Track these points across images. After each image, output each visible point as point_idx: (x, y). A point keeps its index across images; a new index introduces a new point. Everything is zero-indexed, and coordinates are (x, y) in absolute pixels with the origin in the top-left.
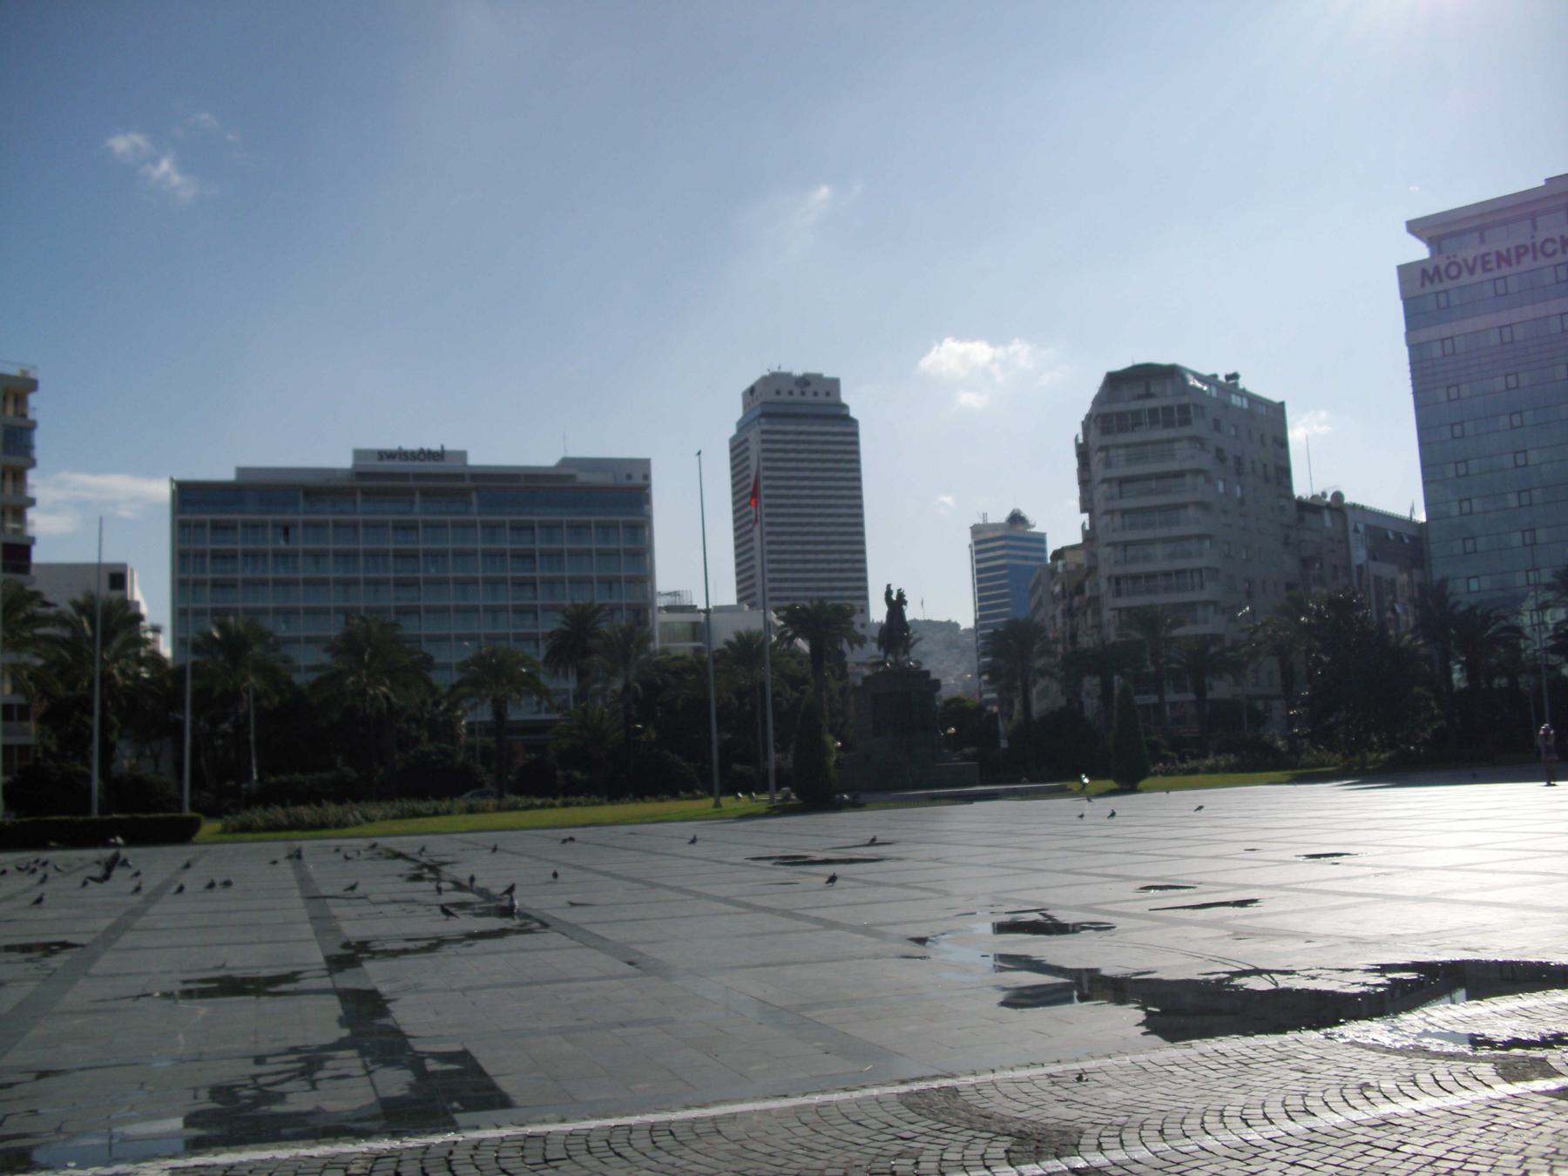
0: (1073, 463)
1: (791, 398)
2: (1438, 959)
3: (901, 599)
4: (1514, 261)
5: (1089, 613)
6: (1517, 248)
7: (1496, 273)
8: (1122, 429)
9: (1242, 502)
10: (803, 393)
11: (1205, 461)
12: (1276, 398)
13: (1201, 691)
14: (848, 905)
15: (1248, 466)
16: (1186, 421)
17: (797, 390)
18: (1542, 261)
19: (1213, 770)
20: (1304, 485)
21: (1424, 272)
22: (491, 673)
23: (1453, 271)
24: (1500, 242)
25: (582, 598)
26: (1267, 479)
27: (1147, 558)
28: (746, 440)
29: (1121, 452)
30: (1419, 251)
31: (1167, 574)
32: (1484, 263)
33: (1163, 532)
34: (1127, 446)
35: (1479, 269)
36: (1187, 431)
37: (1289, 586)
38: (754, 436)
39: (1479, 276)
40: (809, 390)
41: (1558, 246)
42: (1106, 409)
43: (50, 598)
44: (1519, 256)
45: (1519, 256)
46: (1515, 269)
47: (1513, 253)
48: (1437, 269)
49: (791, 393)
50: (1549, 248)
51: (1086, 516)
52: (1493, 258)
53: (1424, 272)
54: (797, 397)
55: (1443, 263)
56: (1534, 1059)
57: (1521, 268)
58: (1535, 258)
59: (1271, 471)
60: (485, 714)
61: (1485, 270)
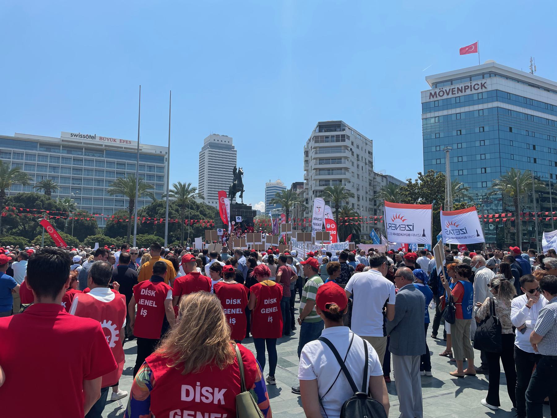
4: (463, 91)
7: (457, 95)
14: (449, 394)
16: (344, 141)
18: (474, 91)
21: (431, 94)
23: (441, 94)
32: (453, 91)
35: (451, 93)
38: (207, 152)
43: (436, 343)
45: (465, 89)
48: (435, 93)
52: (456, 90)
53: (431, 94)
57: (466, 94)
58: (471, 90)
61: (453, 94)
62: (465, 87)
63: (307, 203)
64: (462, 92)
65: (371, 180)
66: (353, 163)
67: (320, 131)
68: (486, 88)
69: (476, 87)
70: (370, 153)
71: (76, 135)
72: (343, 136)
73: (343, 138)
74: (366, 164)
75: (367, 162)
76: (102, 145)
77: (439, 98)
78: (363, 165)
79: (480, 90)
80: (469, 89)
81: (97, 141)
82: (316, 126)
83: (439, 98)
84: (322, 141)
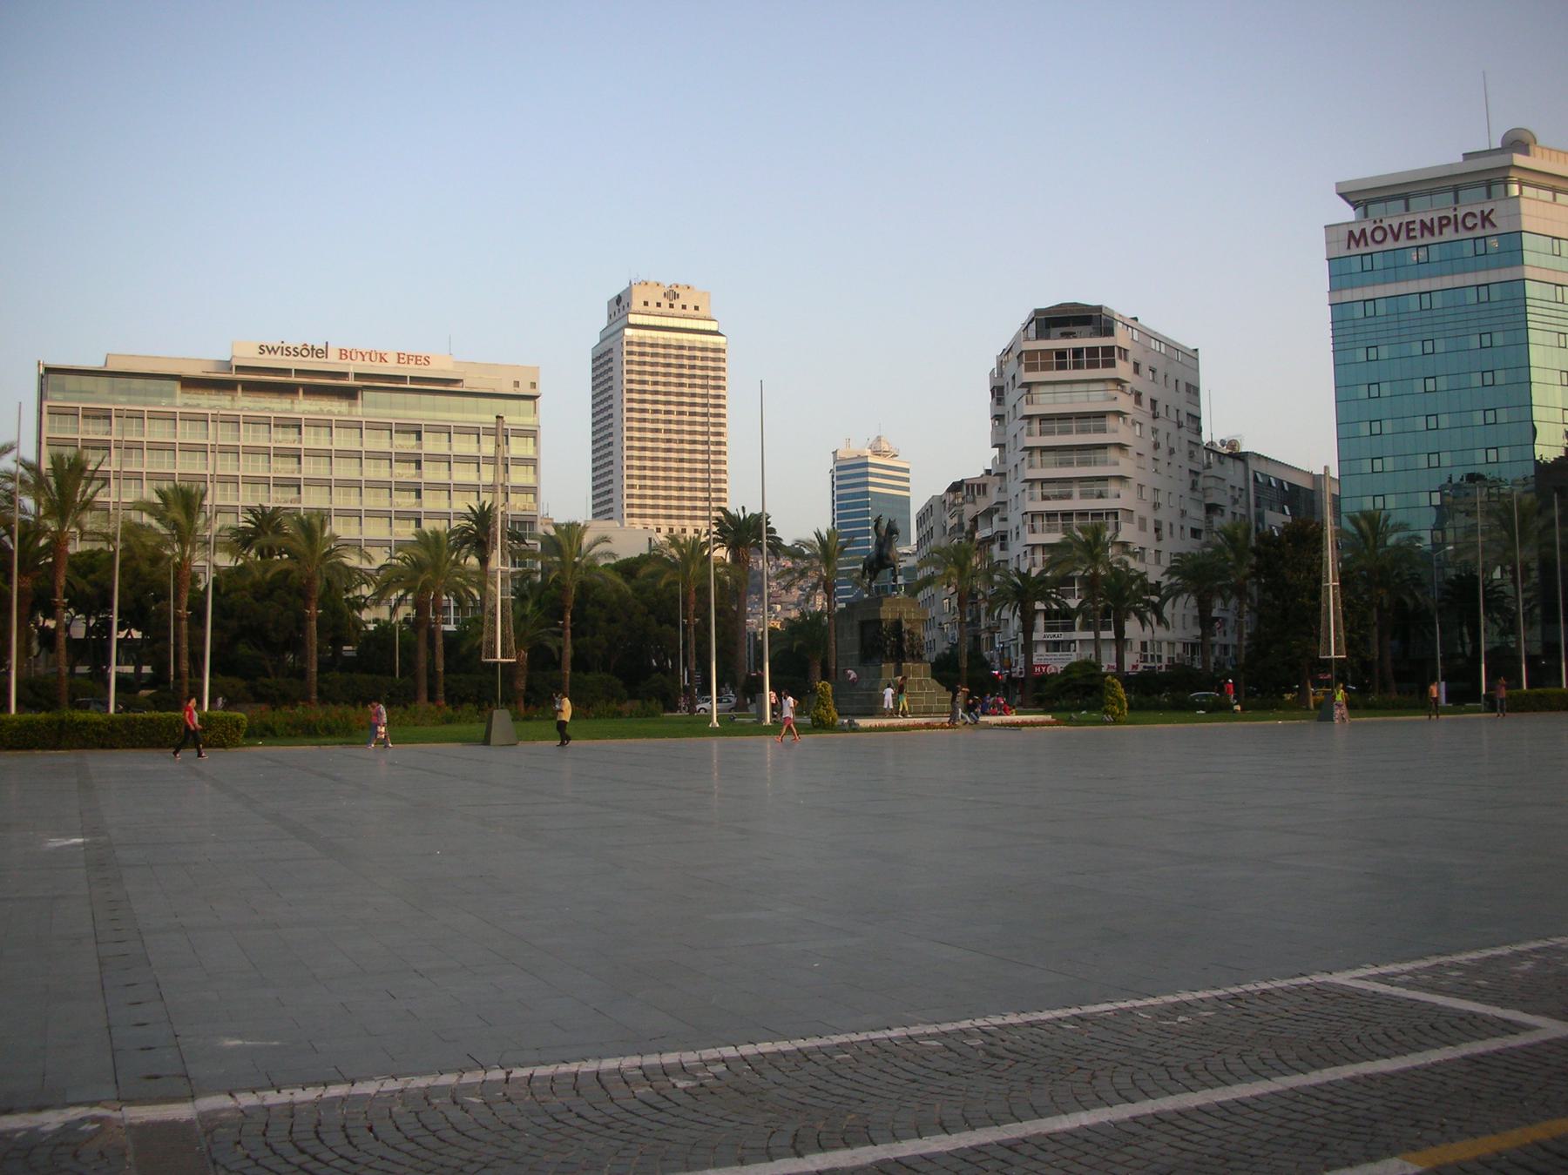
2: (632, 741)
4: (1436, 230)
6: (1440, 219)
7: (1420, 242)
10: (671, 306)
12: (1187, 341)
16: (1111, 364)
17: (665, 303)
18: (1463, 234)
19: (1159, 707)
20: (1214, 430)
21: (1351, 233)
23: (1379, 236)
24: (1424, 211)
25: (186, 466)
28: (610, 350)
30: (1346, 214)
32: (1409, 230)
35: (1403, 235)
39: (1403, 242)
40: (678, 304)
44: (1441, 227)
45: (1441, 227)
47: (1436, 224)
48: (1363, 232)
49: (659, 305)
50: (1469, 223)
52: (1417, 226)
53: (1351, 233)
55: (1369, 228)
61: (1409, 238)
62: (1440, 219)
63: (1003, 548)
64: (1432, 234)
65: (1197, 474)
66: (1138, 395)
67: (1041, 334)
68: (1493, 225)
69: (1469, 223)
70: (1193, 390)
71: (273, 350)
72: (1109, 351)
73: (1108, 356)
74: (1180, 426)
75: (1183, 418)
76: (344, 375)
77: (1373, 248)
78: (1172, 428)
79: (1479, 232)
80: (1452, 227)
81: (333, 363)
82: (1024, 317)
83: (1373, 248)
84: (1046, 367)
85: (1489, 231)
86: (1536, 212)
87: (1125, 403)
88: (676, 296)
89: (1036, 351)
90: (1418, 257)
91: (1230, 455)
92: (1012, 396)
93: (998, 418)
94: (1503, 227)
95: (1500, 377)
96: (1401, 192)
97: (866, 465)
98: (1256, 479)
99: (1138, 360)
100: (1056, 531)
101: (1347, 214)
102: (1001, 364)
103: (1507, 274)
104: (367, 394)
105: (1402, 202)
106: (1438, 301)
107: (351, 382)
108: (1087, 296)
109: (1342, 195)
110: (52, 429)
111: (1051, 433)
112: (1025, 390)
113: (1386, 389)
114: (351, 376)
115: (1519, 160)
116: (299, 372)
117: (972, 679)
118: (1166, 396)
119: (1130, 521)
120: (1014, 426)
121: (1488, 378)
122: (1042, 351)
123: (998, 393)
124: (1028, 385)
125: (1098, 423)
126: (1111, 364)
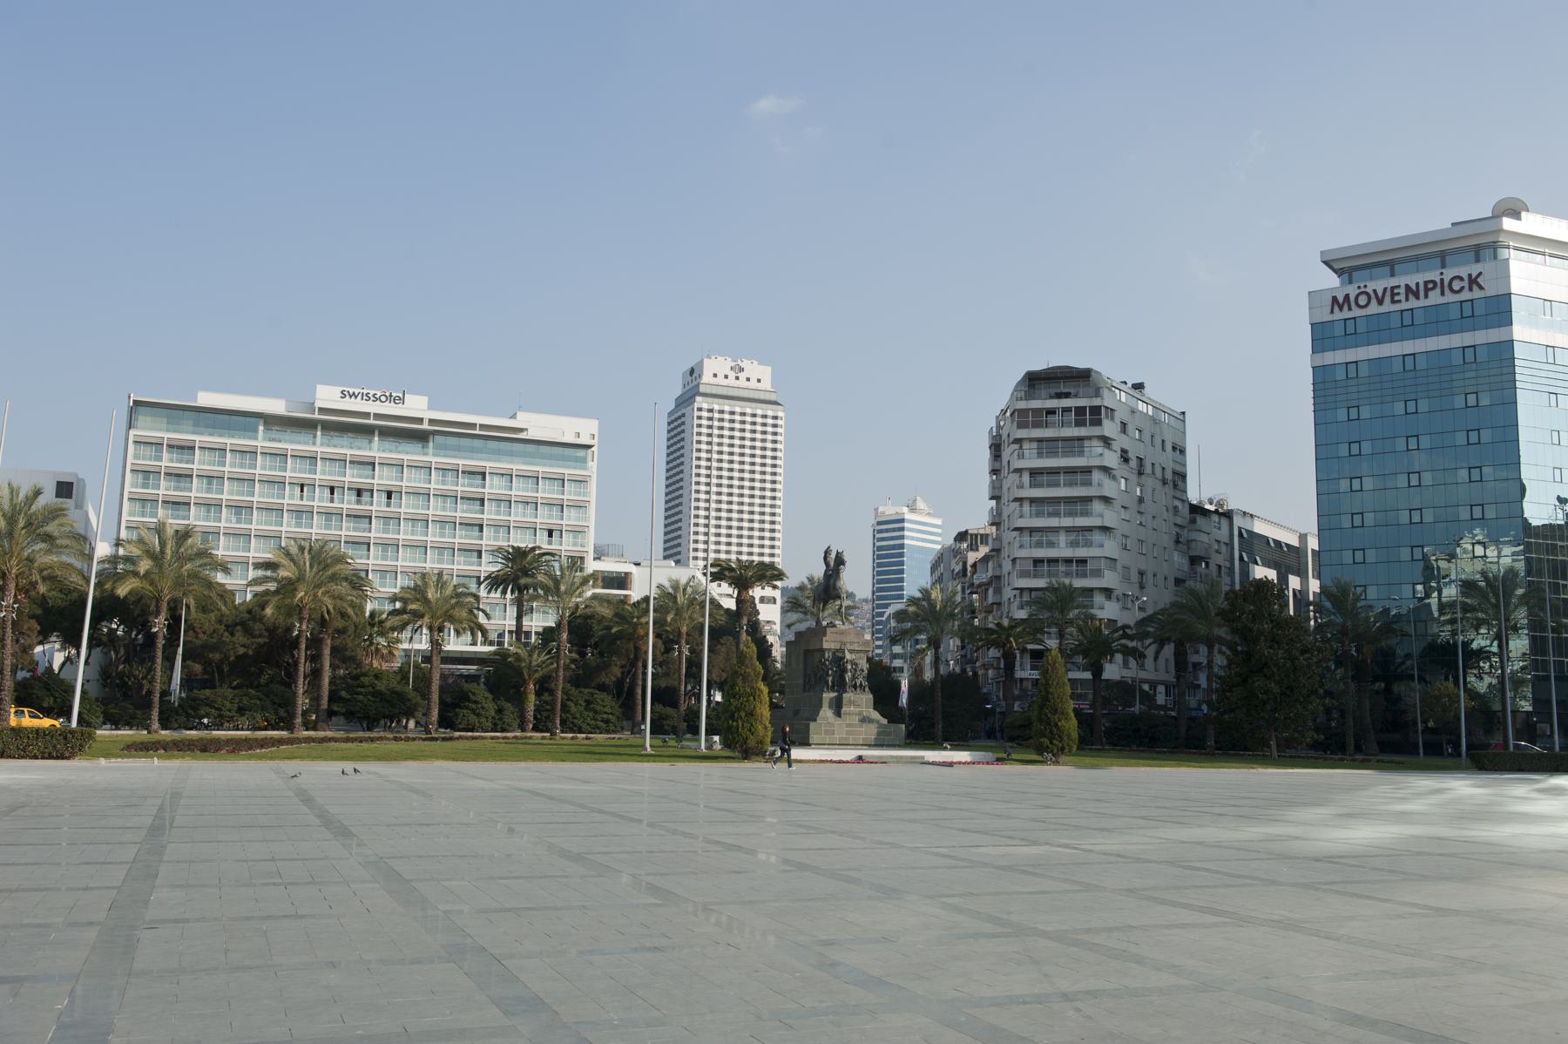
0: (986, 454)
1: (725, 382)
3: (840, 561)
4: (1422, 294)
5: (991, 591)
6: (1426, 283)
7: (1404, 306)
8: (1037, 425)
9: (1141, 500)
11: (1111, 459)
13: (1097, 671)
15: (1148, 469)
17: (732, 375)
18: (1450, 297)
20: (1196, 492)
21: (1335, 299)
22: (428, 604)
23: (1363, 300)
26: (1164, 482)
27: (1051, 545)
29: (1035, 445)
31: (1068, 561)
32: (1393, 295)
33: (1067, 522)
34: (1039, 440)
35: (1387, 299)
36: (1095, 431)
37: (1178, 582)
40: (742, 376)
41: (1466, 284)
42: (1022, 405)
44: (1427, 290)
45: (1427, 290)
46: (1422, 303)
48: (1347, 297)
51: (994, 502)
52: (1402, 290)
53: (1335, 299)
54: (731, 381)
56: (130, 725)
58: (1443, 294)
59: (1169, 476)
60: (422, 644)
61: (1393, 302)
62: (1426, 283)
64: (1417, 297)
67: (1029, 396)
68: (1481, 288)
70: (1180, 450)
72: (1096, 410)
77: (1356, 312)
79: (1466, 295)
80: (1438, 290)
83: (1356, 312)
85: (1477, 294)
86: (1526, 277)
87: (1111, 459)
88: (742, 370)
89: (1027, 410)
90: (1404, 347)
91: (1216, 511)
92: (1008, 452)
93: (994, 472)
94: (1490, 291)
95: (1486, 436)
96: (1386, 260)
97: (903, 521)
98: (1240, 534)
99: (1126, 420)
100: (1042, 576)
101: (1331, 281)
102: (998, 420)
103: (1493, 335)
104: (438, 439)
105: (1387, 269)
106: (1422, 363)
107: (425, 426)
108: (1077, 360)
109: (1326, 263)
110: (136, 457)
111: (1041, 486)
112: (1016, 446)
113: (1367, 448)
114: (426, 422)
115: (1508, 224)
116: (377, 416)
117: (937, 713)
118: (1153, 456)
119: (1113, 569)
120: (1010, 480)
121: (1473, 437)
122: (1034, 410)
123: (996, 449)
124: (1019, 441)
125: (1085, 477)
126: (1099, 423)
